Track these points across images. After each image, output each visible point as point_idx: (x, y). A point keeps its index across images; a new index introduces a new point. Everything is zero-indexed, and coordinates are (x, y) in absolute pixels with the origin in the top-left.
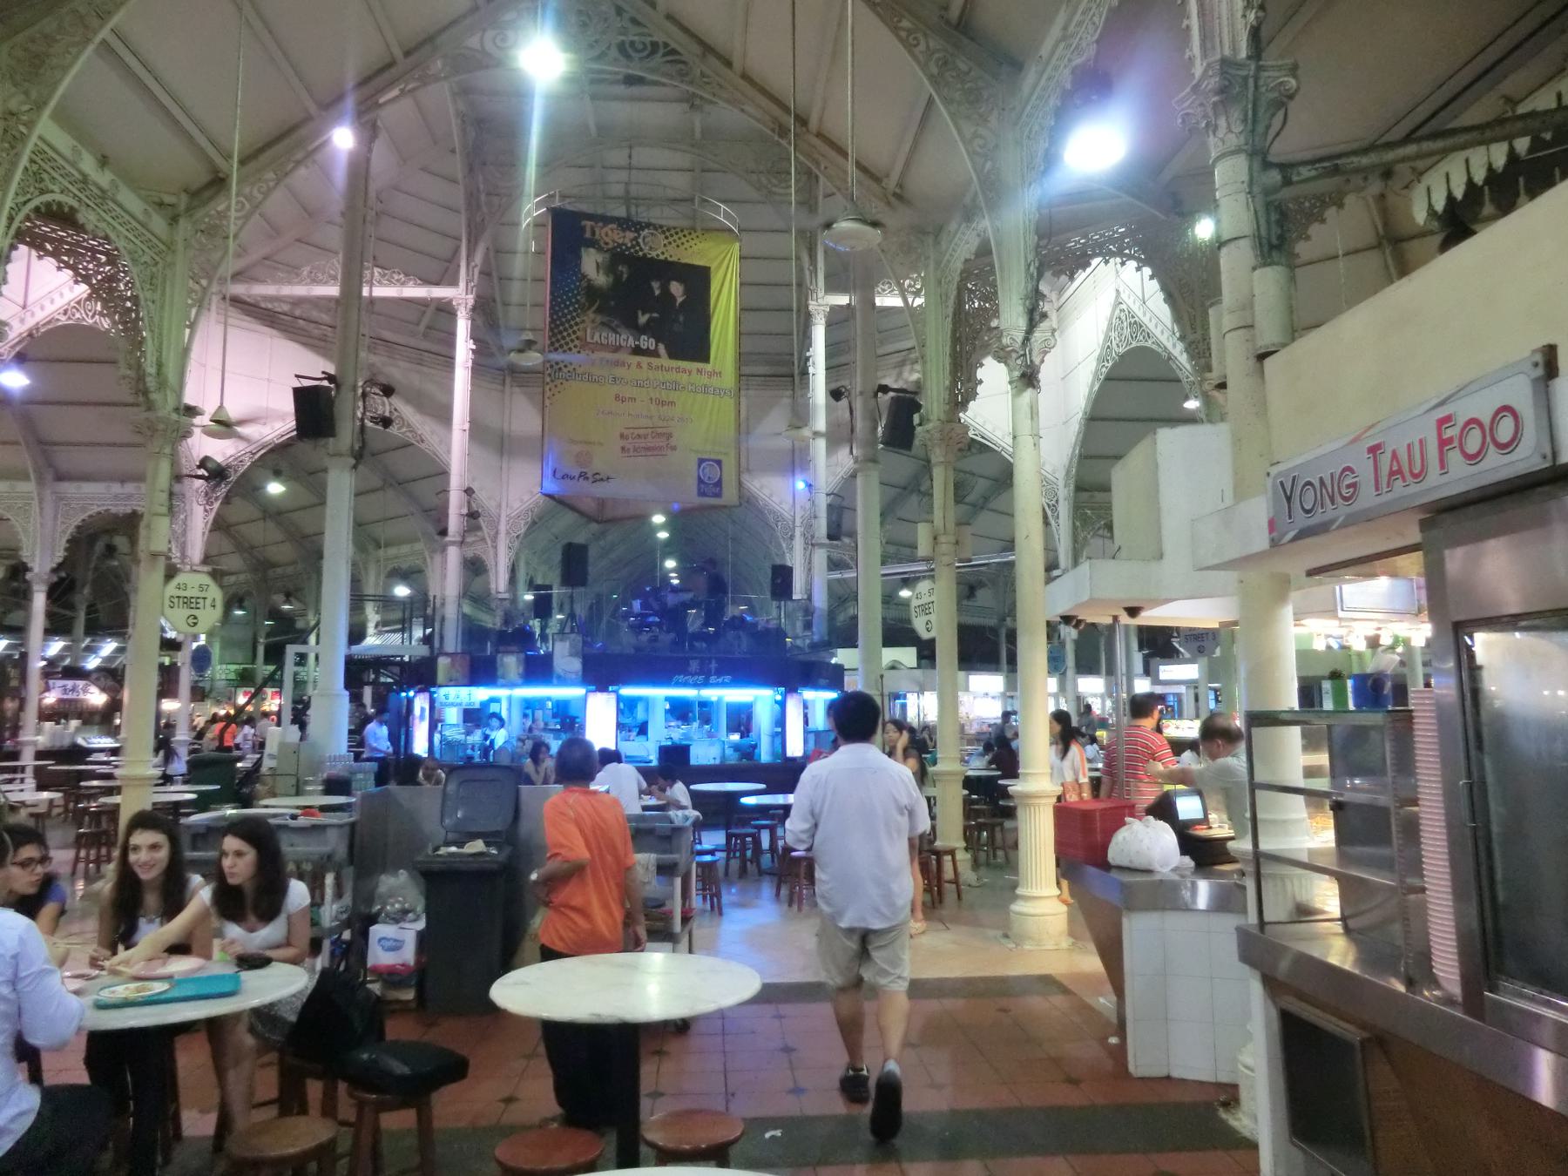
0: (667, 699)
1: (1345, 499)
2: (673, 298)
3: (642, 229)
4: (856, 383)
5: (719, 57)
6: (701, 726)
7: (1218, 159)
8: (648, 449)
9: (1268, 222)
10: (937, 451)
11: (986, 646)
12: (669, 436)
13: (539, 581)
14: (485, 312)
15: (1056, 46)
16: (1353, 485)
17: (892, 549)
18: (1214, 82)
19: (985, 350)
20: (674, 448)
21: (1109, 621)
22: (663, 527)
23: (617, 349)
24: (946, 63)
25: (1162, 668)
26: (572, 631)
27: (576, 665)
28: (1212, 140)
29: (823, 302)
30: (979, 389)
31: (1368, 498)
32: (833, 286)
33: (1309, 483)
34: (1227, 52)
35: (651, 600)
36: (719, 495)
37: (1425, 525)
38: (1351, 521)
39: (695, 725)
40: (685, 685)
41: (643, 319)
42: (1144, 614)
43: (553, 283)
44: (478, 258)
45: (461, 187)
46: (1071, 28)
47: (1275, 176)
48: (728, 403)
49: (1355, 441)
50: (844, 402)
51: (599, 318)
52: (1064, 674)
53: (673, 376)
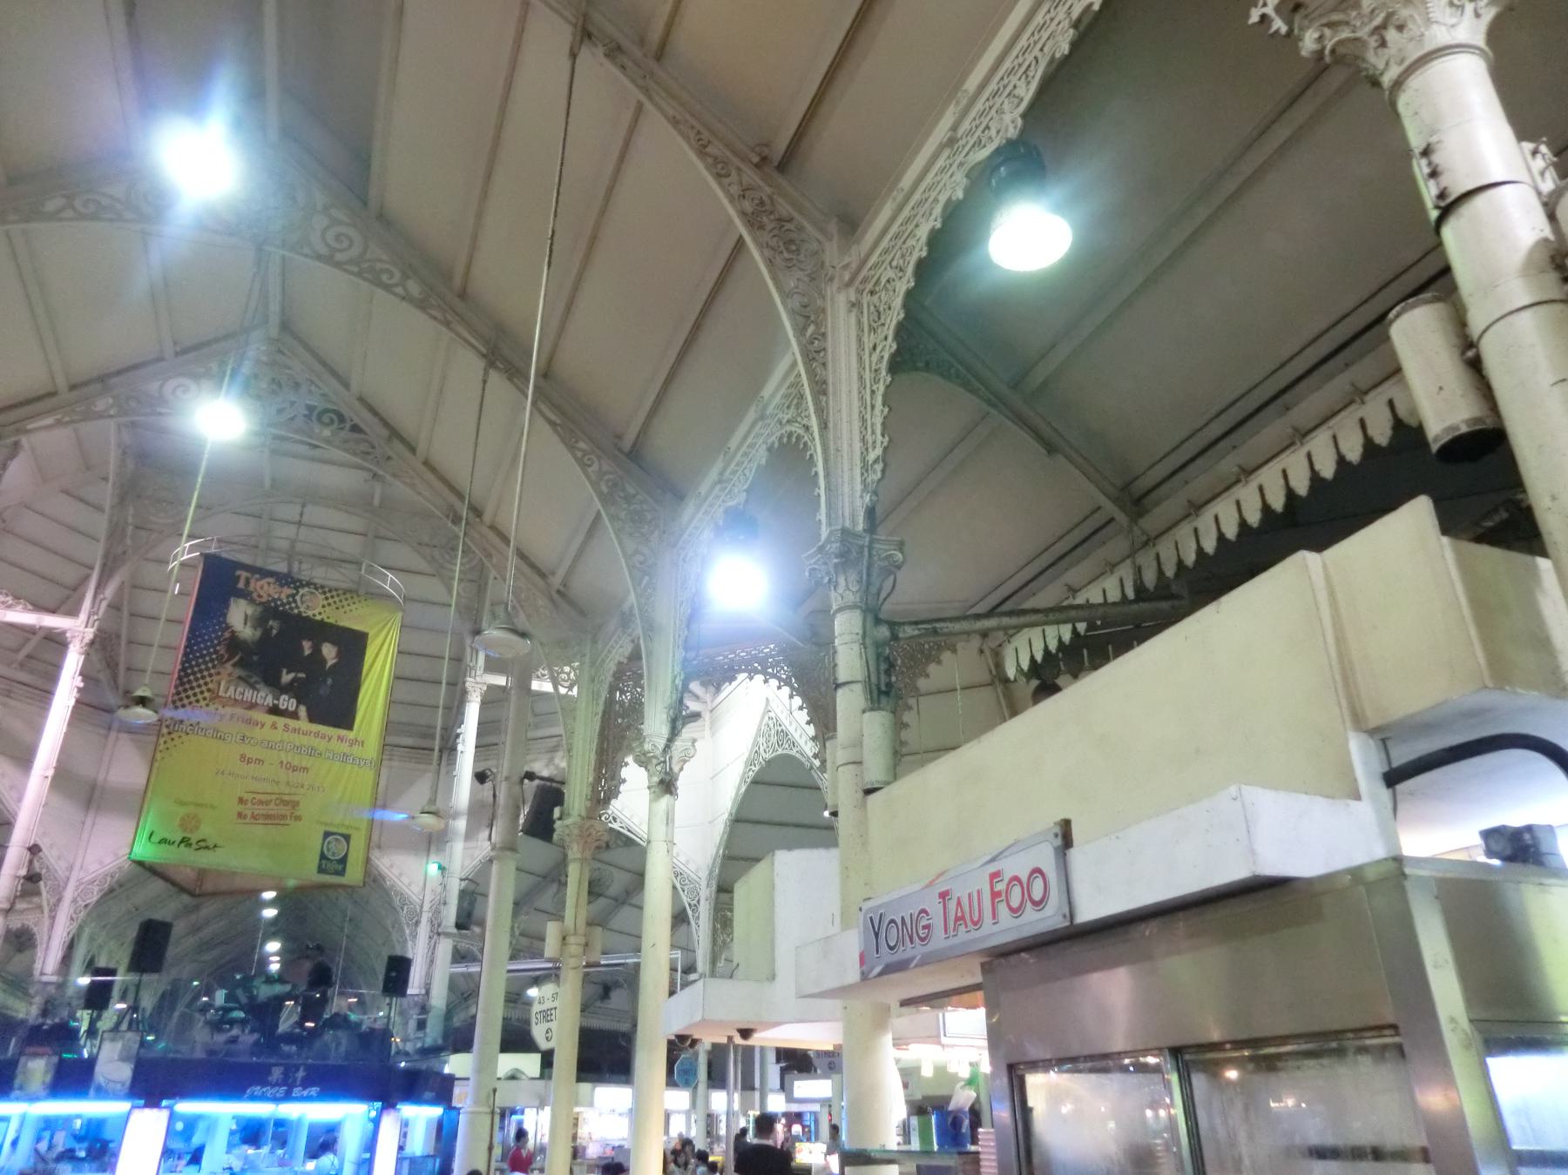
0: (237, 1119)
1: (922, 939)
2: (324, 661)
3: (303, 586)
4: (504, 767)
5: (402, 440)
6: (272, 1151)
7: (840, 610)
8: (268, 817)
9: (878, 670)
10: (575, 847)
11: (605, 1056)
12: (295, 804)
13: (102, 963)
14: (103, 647)
15: (712, 488)
16: (927, 927)
17: (524, 941)
18: (835, 547)
19: (630, 750)
20: (298, 818)
21: (724, 1040)
22: (272, 903)
23: (252, 706)
24: (615, 485)
25: (797, 1083)
26: (130, 1028)
27: (125, 1072)
28: (833, 594)
29: (480, 682)
30: (622, 788)
31: (938, 941)
32: (493, 666)
33: (892, 921)
34: (848, 524)
35: (239, 992)
36: (342, 873)
37: (986, 968)
38: (925, 961)
39: (265, 1150)
40: (262, 1098)
41: (287, 678)
42: (756, 1035)
43: (192, 630)
44: (109, 591)
45: (106, 516)
46: (727, 474)
47: (884, 632)
48: (369, 775)
49: (931, 884)
50: (488, 785)
51: (239, 672)
52: (696, 1088)
53: (305, 740)
